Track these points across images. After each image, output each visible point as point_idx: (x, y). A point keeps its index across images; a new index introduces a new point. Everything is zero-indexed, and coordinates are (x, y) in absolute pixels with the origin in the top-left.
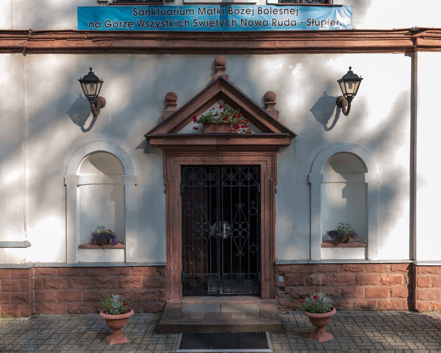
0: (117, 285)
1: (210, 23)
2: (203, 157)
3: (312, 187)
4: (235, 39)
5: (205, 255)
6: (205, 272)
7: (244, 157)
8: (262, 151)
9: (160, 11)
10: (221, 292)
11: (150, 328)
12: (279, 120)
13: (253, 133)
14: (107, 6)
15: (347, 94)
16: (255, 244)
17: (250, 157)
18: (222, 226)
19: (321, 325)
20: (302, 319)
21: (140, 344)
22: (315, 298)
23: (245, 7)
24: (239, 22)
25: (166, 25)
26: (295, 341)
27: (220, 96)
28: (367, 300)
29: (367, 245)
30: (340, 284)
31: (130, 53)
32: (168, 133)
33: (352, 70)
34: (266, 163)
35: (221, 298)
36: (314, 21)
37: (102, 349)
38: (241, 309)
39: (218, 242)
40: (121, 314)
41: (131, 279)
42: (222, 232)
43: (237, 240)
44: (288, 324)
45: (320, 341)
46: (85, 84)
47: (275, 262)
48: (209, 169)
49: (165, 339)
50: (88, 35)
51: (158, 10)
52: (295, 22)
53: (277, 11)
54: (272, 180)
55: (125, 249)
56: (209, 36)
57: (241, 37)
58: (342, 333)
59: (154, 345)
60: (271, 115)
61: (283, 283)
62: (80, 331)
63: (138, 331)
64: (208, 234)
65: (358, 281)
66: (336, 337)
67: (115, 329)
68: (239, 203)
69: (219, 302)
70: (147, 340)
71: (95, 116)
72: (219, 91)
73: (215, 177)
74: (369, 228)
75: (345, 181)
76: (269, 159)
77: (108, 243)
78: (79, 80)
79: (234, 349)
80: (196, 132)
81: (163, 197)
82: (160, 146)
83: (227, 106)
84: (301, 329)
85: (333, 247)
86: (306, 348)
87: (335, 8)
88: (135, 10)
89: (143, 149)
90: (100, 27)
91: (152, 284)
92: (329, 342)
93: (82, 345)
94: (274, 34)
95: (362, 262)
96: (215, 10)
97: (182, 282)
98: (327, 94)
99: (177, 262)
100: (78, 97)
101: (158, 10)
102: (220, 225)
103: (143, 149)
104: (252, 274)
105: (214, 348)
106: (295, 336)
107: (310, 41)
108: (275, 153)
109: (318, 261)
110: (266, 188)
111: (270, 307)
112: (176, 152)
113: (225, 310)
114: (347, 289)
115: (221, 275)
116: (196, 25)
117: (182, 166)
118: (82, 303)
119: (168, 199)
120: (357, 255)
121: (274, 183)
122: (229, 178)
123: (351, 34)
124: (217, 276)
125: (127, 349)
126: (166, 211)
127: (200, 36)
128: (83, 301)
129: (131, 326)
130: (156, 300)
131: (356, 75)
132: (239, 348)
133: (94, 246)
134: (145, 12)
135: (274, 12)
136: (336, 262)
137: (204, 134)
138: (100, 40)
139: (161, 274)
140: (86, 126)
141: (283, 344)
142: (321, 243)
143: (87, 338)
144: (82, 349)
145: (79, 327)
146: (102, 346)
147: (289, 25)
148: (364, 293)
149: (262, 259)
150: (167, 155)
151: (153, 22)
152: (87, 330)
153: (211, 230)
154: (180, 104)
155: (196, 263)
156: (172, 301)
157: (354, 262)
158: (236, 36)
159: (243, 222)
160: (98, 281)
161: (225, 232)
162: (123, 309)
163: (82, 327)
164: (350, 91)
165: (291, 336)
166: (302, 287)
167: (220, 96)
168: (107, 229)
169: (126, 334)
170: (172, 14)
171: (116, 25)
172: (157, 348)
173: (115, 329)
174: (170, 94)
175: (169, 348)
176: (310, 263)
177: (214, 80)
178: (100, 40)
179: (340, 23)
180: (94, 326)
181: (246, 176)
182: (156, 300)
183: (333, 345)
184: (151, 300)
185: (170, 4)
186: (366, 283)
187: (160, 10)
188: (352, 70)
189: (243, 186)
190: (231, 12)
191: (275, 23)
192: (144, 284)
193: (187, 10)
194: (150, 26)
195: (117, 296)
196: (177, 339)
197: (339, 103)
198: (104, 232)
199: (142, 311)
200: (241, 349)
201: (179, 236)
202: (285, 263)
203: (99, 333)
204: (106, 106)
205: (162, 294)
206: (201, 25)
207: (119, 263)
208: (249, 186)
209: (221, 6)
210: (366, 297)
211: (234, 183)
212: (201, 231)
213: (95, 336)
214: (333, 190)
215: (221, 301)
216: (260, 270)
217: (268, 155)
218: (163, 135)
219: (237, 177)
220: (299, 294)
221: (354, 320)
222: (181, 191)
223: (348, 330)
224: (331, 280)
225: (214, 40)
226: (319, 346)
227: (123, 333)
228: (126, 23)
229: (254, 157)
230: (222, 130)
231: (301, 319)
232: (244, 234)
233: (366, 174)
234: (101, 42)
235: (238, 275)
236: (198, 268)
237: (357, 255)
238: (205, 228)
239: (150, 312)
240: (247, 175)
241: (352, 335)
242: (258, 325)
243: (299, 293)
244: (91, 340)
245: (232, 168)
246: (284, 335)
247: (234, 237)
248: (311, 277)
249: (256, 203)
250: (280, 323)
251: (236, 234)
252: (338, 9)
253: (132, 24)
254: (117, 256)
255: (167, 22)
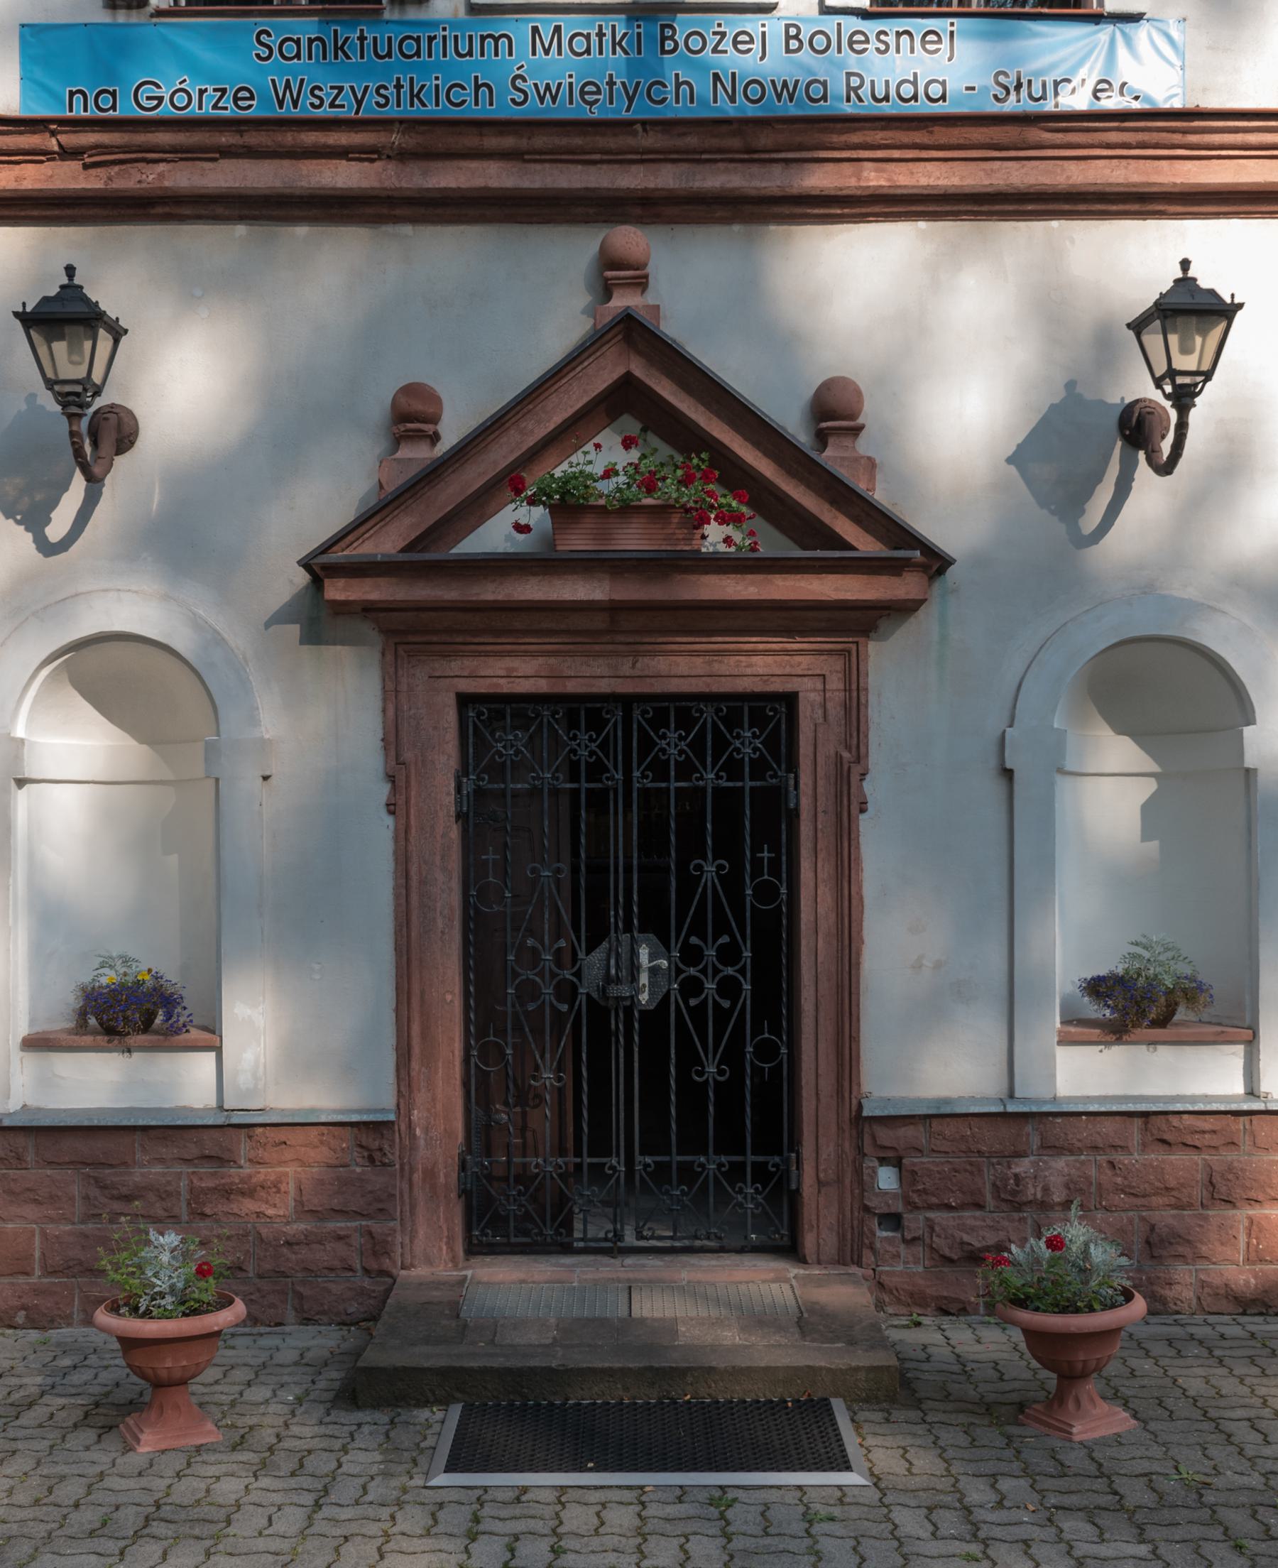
0: (184, 1205)
1: (582, 93)
2: (552, 661)
3: (1014, 785)
4: (687, 152)
5: (560, 1079)
6: (562, 1152)
7: (726, 659)
8: (803, 633)
9: (369, 41)
10: (630, 1239)
11: (322, 1384)
12: (880, 496)
13: (763, 551)
14: (143, 20)
15: (1172, 373)
16: (776, 1030)
17: (754, 659)
18: (634, 954)
19: (1080, 1366)
20: (990, 1344)
21: (271, 1449)
22: (1055, 1243)
23: (728, 23)
24: (703, 87)
25: (393, 100)
26: (963, 1440)
27: (624, 400)
28: (1258, 1267)
29: (1255, 1035)
30: (1139, 1201)
31: (241, 219)
32: (403, 551)
33: (1191, 274)
34: (820, 686)
35: (629, 1261)
36: (1024, 81)
37: (98, 1469)
38: (718, 1304)
39: (616, 1023)
40: (185, 1315)
41: (242, 1181)
42: (634, 979)
43: (698, 1014)
44: (925, 1366)
45: (1077, 1438)
46: (49, 341)
47: (860, 1106)
48: (583, 711)
49: (383, 1429)
50: (63, 138)
51: (362, 38)
52: (943, 83)
53: (867, 41)
54: (846, 755)
55: (219, 1050)
56: (577, 141)
57: (714, 142)
58: (1169, 1402)
59: (333, 1456)
60: (843, 473)
61: (895, 1196)
62: (16, 1396)
63: (269, 1394)
64: (574, 988)
65: (1221, 1191)
66: (1145, 1422)
67: (160, 1384)
68: (705, 858)
69: (622, 1276)
70: (306, 1431)
71: (94, 481)
72: (620, 371)
73: (604, 746)
74: (1261, 958)
75: (1155, 768)
76: (832, 667)
77: (147, 1026)
78: (16, 314)
79: (695, 1470)
80: (522, 544)
81: (383, 828)
82: (368, 609)
83: (654, 440)
84: (982, 1388)
85: (1108, 1044)
86: (1016, 1466)
87: (1111, 27)
88: (264, 38)
89: (298, 626)
90: (114, 108)
91: (336, 1203)
92: (1118, 1440)
93: (14, 1452)
94: (855, 130)
95: (1234, 1107)
96: (601, 35)
97: (465, 1193)
98: (1079, 390)
99: (439, 1106)
100: (24, 407)
101: (362, 38)
102: (624, 950)
103: (298, 626)
104: (761, 1159)
105: (601, 1467)
106: (962, 1418)
107: (1010, 164)
108: (861, 640)
109: (1045, 1102)
110: (820, 790)
111: (844, 1294)
112: (435, 639)
113: (649, 1307)
114: (1171, 1221)
115: (630, 1162)
116: (519, 97)
117: (465, 701)
118: (33, 1280)
119: (402, 837)
120: (1212, 1077)
121: (856, 770)
122: (663, 751)
123: (1185, 132)
124: (612, 1168)
125: (212, 1471)
126: (396, 888)
127: (540, 141)
128: (38, 1272)
129: (240, 1375)
130: (351, 1269)
131: (1212, 292)
132: (718, 1469)
133: (88, 1039)
134: (304, 44)
135: (851, 43)
136: (1123, 1108)
137: (554, 556)
138: (114, 163)
139: (371, 1160)
140: (57, 528)
141: (912, 1450)
142: (1058, 1025)
143: (40, 1426)
144: (9, 1471)
145: (14, 1381)
146: (101, 1458)
147: (915, 97)
148: (1243, 1238)
149: (804, 1094)
150: (400, 649)
151: (341, 89)
152: (42, 1394)
153: (585, 971)
154: (452, 431)
155: (524, 1114)
156: (420, 1272)
157: (1200, 1107)
158: (692, 141)
159: (725, 939)
160: (105, 1187)
161: (644, 979)
162: (196, 1296)
163: (25, 1380)
164: (1184, 363)
165: (941, 1417)
166: (978, 1213)
167: (624, 400)
168: (144, 967)
169: (213, 1409)
170: (418, 54)
171: (181, 100)
172: (344, 1469)
173: (160, 1384)
174: (411, 390)
175: (401, 1468)
176: (1010, 1109)
177: (599, 327)
178: (114, 163)
179: (1131, 91)
180: (76, 1378)
181: (737, 743)
182: (351, 1269)
183: (1138, 1454)
184: (331, 1269)
185: (413, 14)
186: (1252, 1194)
187: (370, 37)
188: (1191, 274)
189: (724, 783)
190: (669, 45)
191: (856, 89)
192: (299, 1202)
193: (483, 38)
194: (327, 104)
195: (171, 1239)
196: (436, 1428)
197: (1136, 428)
198: (130, 979)
199: (291, 1315)
200: (727, 1470)
201: (449, 997)
202: (904, 1112)
203: (97, 1405)
204: (138, 443)
205: (378, 1247)
206: (542, 99)
207: (192, 1110)
208: (749, 784)
209: (630, 20)
210: (1253, 1256)
211: (685, 770)
212: (541, 974)
213: (78, 1414)
214: (1109, 793)
215: (631, 1275)
216: (795, 1144)
217: (830, 652)
218: (379, 558)
219: (698, 746)
220: (962, 1243)
221: (1211, 1352)
222: (459, 803)
223: (1191, 1393)
224: (1099, 1185)
225: (597, 157)
226: (1075, 1459)
227: (201, 1405)
228: (224, 91)
229: (770, 659)
230: (633, 539)
231: (978, 1348)
232: (729, 988)
233: (1248, 731)
234: (117, 168)
235: (702, 1165)
236: (529, 1135)
237: (1212, 1077)
238: (559, 963)
239: (325, 1319)
240: (738, 736)
241: (1213, 1413)
242: (797, 1369)
243: (966, 1238)
244: (57, 1434)
245: (677, 709)
246: (914, 1415)
247: (687, 1004)
248: (1017, 1170)
249: (779, 858)
250: (894, 1362)
251: (691, 987)
252: (1123, 33)
253: (252, 98)
254: (188, 1083)
255: (398, 87)
